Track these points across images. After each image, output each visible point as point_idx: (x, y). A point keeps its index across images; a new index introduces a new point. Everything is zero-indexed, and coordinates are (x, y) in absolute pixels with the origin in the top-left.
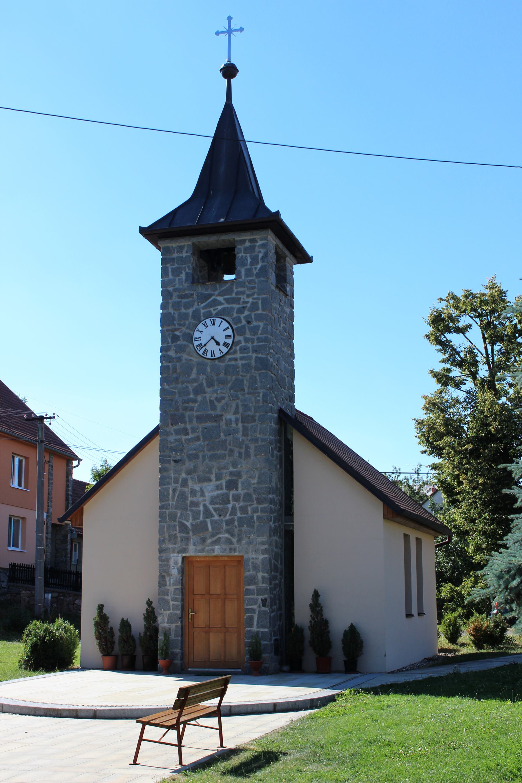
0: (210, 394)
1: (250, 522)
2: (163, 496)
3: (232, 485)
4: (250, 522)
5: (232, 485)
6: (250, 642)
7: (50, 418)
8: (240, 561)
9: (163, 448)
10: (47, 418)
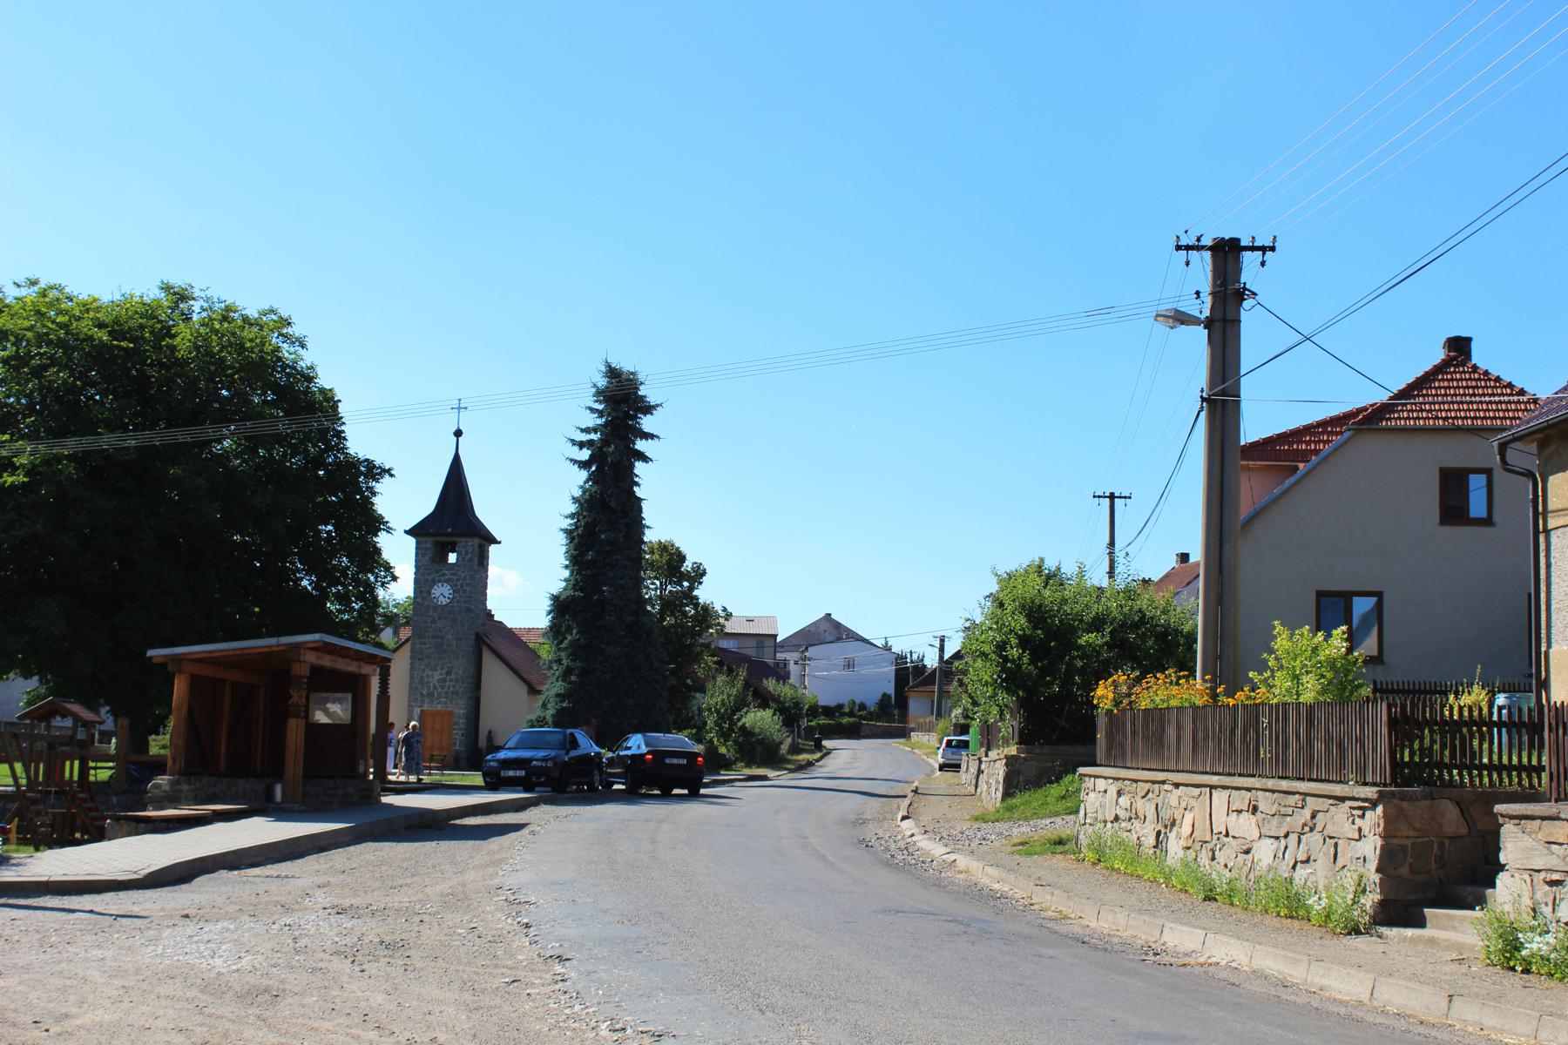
0: (439, 624)
1: (457, 693)
2: (412, 677)
3: (449, 673)
4: (457, 693)
5: (449, 673)
6: (102, 344)
7: (1263, 249)
8: (451, 714)
9: (413, 651)
10: (1253, 248)
